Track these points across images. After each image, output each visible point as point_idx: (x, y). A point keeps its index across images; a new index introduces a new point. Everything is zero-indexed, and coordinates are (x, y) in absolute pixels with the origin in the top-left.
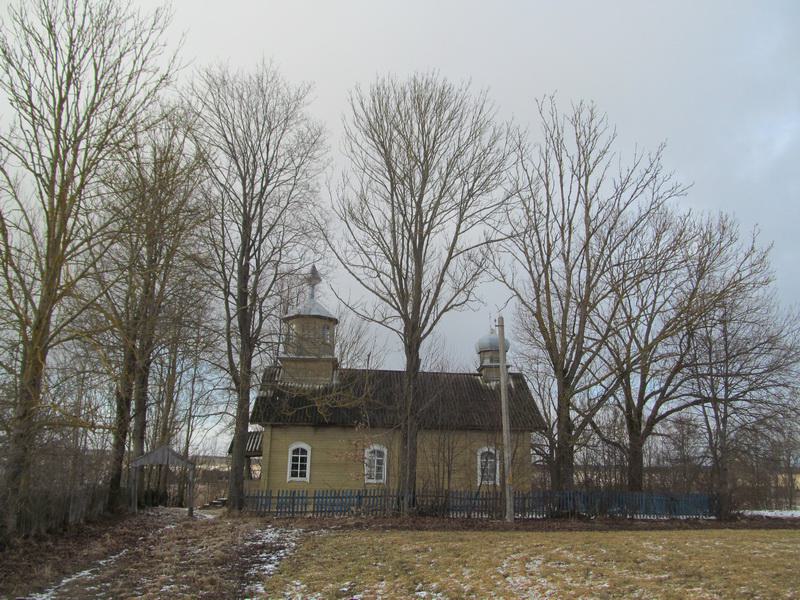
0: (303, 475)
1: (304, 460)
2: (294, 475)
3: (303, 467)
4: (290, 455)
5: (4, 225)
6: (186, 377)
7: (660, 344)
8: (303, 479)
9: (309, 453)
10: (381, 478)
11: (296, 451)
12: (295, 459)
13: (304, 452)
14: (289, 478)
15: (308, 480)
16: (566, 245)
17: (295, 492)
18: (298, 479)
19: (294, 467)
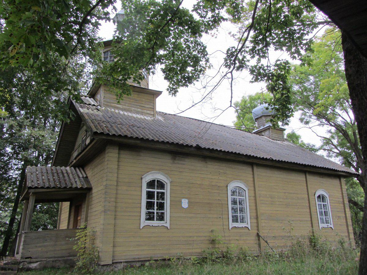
0: (161, 218)
2: (150, 217)
4: (145, 189)
8: (160, 223)
11: (151, 184)
12: (150, 195)
13: (161, 185)
14: (144, 222)
18: (155, 223)
19: (150, 205)
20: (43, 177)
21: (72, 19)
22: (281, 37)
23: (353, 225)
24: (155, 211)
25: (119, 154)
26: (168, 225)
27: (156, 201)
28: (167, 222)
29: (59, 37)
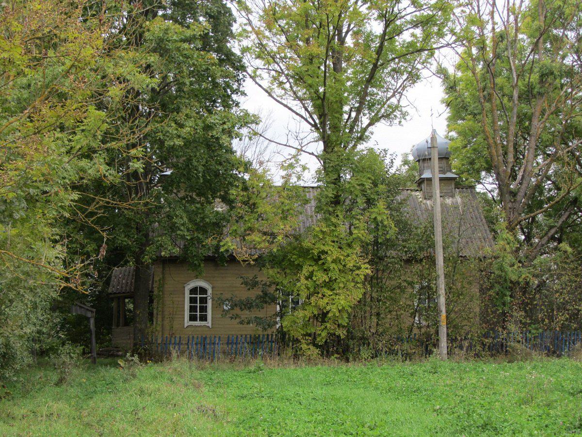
0: (204, 318)
1: (204, 301)
2: (193, 318)
3: (204, 309)
4: (187, 296)
5: (44, 2)
6: (442, 58)
7: (550, 77)
8: (203, 323)
9: (210, 292)
10: (206, 320)
11: (193, 291)
12: (193, 300)
13: (203, 291)
14: (187, 322)
15: (210, 325)
16: (275, 97)
17: (205, 338)
18: (198, 323)
19: (192, 309)
20: (224, 151)
21: (445, 406)
22: (478, 32)
23: (446, 294)
24: (198, 305)
25: (164, 268)
26: (210, 325)
27: (198, 313)
28: (209, 323)
29: (66, 159)
